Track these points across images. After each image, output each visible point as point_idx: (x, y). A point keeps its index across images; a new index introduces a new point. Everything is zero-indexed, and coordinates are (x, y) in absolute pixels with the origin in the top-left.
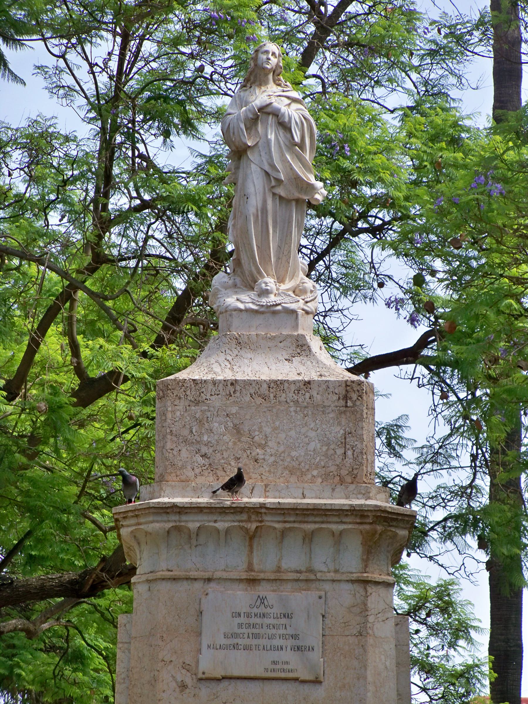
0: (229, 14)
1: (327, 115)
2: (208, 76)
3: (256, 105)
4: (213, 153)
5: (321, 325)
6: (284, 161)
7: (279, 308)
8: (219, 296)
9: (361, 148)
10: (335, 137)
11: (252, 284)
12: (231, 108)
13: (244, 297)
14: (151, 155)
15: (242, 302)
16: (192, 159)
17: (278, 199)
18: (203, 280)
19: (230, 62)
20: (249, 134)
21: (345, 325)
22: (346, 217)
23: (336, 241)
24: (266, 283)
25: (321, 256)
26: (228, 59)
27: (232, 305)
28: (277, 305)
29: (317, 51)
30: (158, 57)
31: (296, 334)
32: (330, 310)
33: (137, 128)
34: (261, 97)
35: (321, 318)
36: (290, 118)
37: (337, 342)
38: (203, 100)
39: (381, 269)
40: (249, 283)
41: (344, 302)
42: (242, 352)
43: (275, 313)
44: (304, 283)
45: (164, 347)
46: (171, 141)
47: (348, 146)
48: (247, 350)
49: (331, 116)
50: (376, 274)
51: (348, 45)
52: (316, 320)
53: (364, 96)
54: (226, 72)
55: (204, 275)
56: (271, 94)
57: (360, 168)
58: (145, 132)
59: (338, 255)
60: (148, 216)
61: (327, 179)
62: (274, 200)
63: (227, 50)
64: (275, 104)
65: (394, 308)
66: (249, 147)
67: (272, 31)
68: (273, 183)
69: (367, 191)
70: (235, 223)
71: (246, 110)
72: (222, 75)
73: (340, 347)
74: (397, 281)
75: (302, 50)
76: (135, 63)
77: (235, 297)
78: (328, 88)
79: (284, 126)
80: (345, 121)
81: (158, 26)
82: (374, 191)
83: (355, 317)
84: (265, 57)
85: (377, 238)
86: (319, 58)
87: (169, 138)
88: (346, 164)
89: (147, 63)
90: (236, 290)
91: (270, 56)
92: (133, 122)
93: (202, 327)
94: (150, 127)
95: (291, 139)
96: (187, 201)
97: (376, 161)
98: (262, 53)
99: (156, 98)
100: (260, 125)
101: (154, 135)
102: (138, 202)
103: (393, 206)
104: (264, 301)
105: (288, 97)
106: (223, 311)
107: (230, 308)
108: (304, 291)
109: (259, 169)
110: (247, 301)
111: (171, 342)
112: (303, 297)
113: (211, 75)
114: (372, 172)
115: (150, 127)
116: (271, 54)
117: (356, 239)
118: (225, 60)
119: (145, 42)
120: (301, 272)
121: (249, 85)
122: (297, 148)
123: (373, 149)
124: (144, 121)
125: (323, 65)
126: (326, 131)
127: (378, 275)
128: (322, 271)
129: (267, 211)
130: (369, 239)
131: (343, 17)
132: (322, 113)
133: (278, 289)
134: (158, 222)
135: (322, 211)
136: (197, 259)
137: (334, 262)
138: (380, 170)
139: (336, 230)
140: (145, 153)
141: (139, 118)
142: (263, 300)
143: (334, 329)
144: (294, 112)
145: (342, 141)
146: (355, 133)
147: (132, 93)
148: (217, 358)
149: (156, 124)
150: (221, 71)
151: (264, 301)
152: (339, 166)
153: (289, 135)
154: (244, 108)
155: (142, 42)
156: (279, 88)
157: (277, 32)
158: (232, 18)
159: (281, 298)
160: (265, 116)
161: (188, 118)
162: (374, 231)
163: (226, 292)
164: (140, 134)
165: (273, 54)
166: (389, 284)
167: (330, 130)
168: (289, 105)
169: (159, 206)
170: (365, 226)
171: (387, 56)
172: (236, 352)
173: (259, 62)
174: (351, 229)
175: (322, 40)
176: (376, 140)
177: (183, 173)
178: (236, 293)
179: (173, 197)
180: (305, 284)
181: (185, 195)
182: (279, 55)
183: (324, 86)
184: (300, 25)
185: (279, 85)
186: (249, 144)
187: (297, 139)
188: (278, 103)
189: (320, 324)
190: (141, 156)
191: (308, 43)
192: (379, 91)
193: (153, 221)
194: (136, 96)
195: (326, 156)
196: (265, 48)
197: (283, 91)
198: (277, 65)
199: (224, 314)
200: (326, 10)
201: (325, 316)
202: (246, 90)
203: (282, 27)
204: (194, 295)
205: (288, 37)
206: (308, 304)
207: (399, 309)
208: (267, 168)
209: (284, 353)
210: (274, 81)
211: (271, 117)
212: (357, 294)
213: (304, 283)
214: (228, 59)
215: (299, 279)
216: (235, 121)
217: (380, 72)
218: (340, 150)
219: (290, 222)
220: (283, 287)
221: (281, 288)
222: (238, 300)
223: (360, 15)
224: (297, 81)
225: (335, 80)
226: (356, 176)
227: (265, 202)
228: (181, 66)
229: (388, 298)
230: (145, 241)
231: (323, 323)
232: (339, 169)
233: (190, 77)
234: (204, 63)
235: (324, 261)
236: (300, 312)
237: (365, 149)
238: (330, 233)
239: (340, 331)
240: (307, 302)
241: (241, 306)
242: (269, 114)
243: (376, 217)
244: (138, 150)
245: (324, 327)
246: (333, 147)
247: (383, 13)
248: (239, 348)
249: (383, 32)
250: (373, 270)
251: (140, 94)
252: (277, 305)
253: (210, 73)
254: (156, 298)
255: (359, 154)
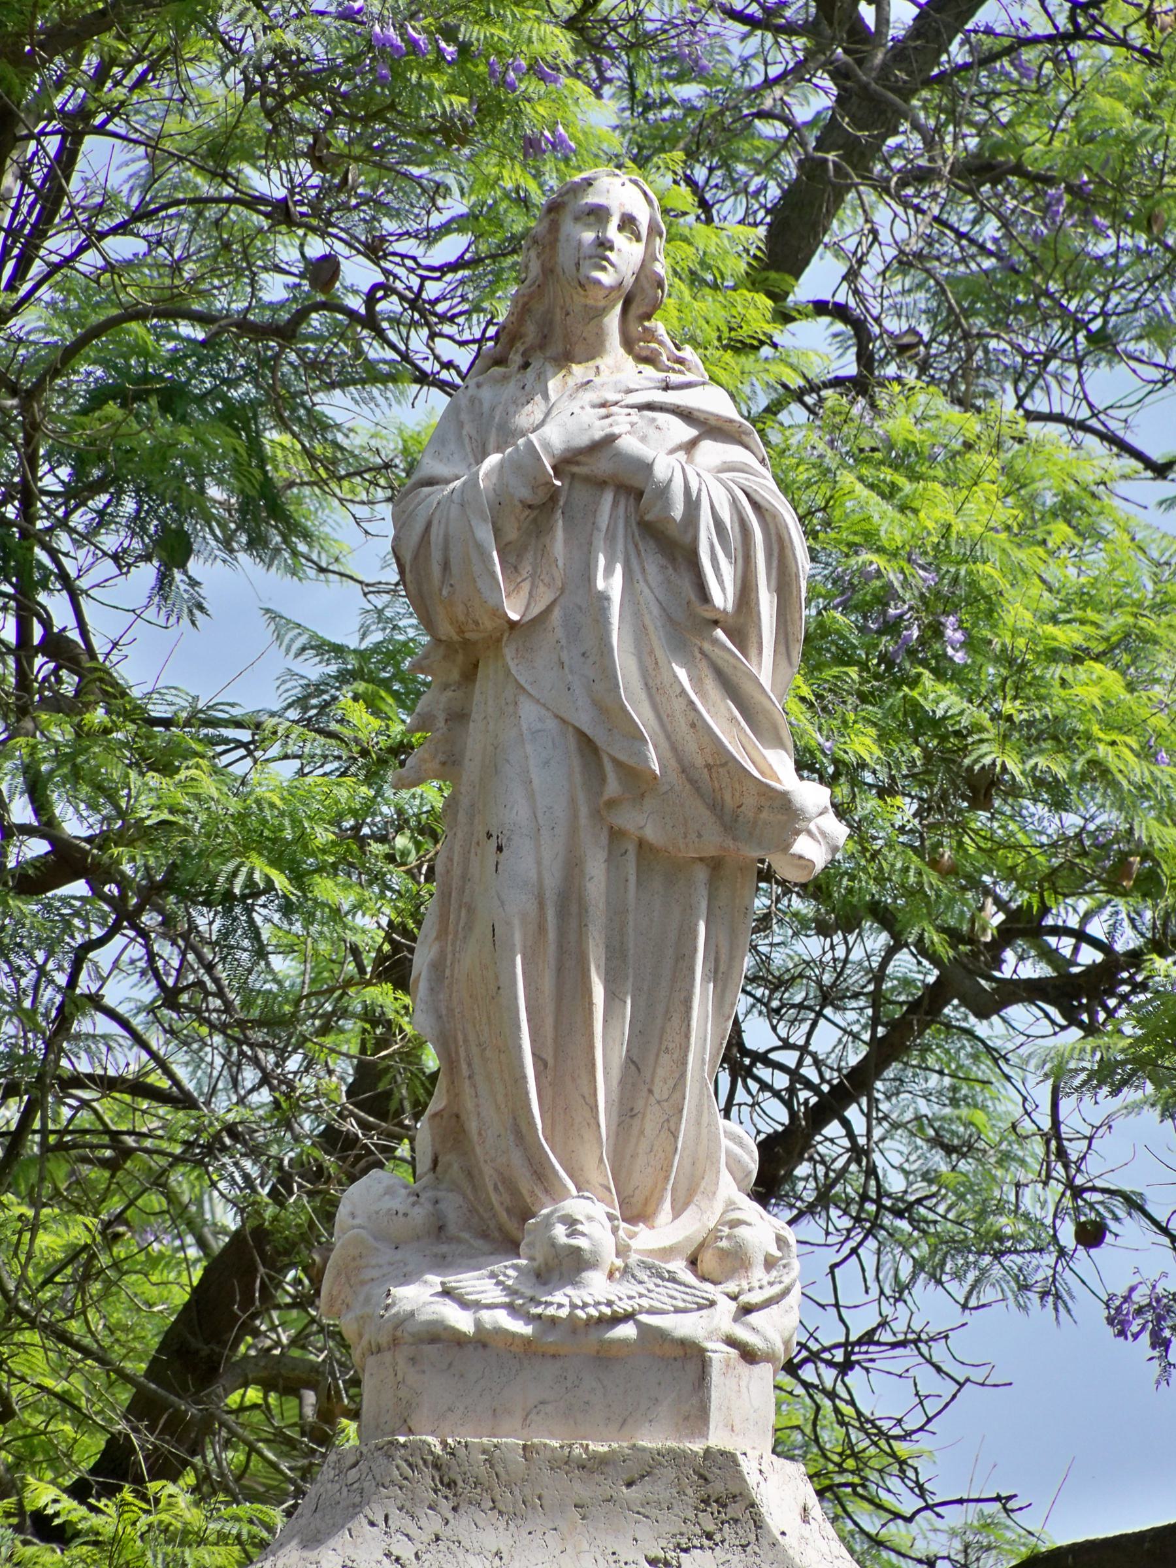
0: (449, 33)
1: (871, 487)
2: (356, 303)
3: (547, 446)
4: (376, 637)
5: (826, 1403)
6: (656, 688)
7: (627, 1331)
8: (369, 1274)
9: (1016, 633)
10: (905, 583)
11: (511, 1226)
12: (437, 454)
13: (476, 1283)
14: (100, 645)
15: (464, 1304)
16: (279, 661)
17: (632, 856)
18: (310, 1194)
19: (451, 247)
20: (511, 568)
21: (932, 1407)
22: (942, 929)
23: (900, 1033)
24: (571, 1222)
25: (831, 1106)
26: (445, 229)
27: (424, 1316)
28: (617, 1319)
29: (839, 200)
30: (142, 214)
31: (697, 1447)
32: (868, 1338)
33: (40, 525)
34: (565, 412)
35: (829, 1376)
36: (692, 505)
37: (894, 1483)
38: (335, 405)
39: (1093, 1166)
40: (492, 1218)
41: (931, 1305)
42: (461, 1526)
43: (607, 1358)
44: (735, 1224)
45: (127, 1494)
46: (194, 583)
47: (960, 626)
48: (480, 1516)
49: (889, 492)
50: (1070, 1184)
51: (980, 171)
52: (806, 1385)
53: (1038, 402)
54: (432, 289)
55: (319, 1174)
56: (612, 397)
57: (1009, 718)
58: (77, 545)
59: (913, 1093)
60: (77, 913)
61: (863, 765)
62: (614, 857)
63: (441, 190)
64: (629, 444)
65: (1145, 1337)
66: (513, 625)
67: (648, 107)
68: (613, 787)
69: (1043, 822)
70: (442, 954)
71: (501, 464)
72: (415, 302)
73: (909, 1503)
74: (1162, 1218)
75: (774, 192)
76: (43, 236)
77: (435, 1281)
78: (883, 362)
79: (665, 542)
80: (950, 517)
81: (152, 68)
82: (1072, 821)
83: (978, 1375)
84: (589, 236)
85: (1080, 1025)
86: (845, 227)
87: (182, 566)
88: (942, 698)
89: (92, 239)
90: (444, 1248)
91: (612, 232)
92: (27, 495)
93: (310, 1397)
94: (103, 518)
95: (693, 596)
96: (244, 849)
97: (1078, 690)
98: (577, 219)
99: (125, 391)
100: (559, 533)
101: (115, 557)
102: (38, 847)
103: (1149, 885)
104: (561, 1301)
105: (686, 415)
106: (384, 1340)
107: (410, 1327)
108: (736, 1260)
109: (551, 724)
110: (486, 1299)
111: (168, 1470)
112: (731, 1287)
113: (371, 299)
114: (1057, 734)
115: (103, 518)
116: (615, 221)
117: (989, 1029)
118: (431, 237)
119: (89, 141)
120: (726, 1178)
121: (516, 359)
122: (719, 633)
123: (1067, 636)
124: (76, 493)
125: (861, 262)
126: (866, 556)
127: (1078, 1192)
128: (839, 1164)
129: (583, 910)
130: (1045, 1027)
131: (957, 52)
132: (847, 479)
133: (622, 1251)
134: (118, 941)
135: (838, 905)
136: (284, 1113)
137: (895, 1126)
138: (1095, 729)
139: (906, 982)
140: (74, 635)
141: (53, 478)
142: (558, 1297)
143: (885, 1425)
144: (710, 480)
145: (937, 603)
146: (988, 568)
147: (20, 372)
148: (350, 1551)
149: (129, 505)
150: (415, 282)
151: (561, 1301)
152: (916, 705)
153: (686, 585)
154: (494, 459)
155: (78, 141)
156: (649, 370)
157: (666, 112)
158: (464, 49)
159: (634, 1289)
160: (582, 494)
161: (268, 481)
162: (1074, 995)
163: (399, 1255)
164: (53, 554)
165: (628, 223)
166: (1129, 1231)
167: (880, 550)
168: (690, 446)
169: (127, 868)
170: (1033, 970)
171: (1149, 222)
172: (432, 1523)
173: (565, 258)
174: (968, 978)
175: (859, 156)
176: (1085, 598)
177: (238, 724)
178: (442, 1264)
179: (186, 831)
180: (742, 1231)
181: (241, 818)
182: (654, 230)
183: (865, 359)
184: (769, 83)
185: (649, 359)
186: (515, 617)
187: (723, 596)
188: (643, 439)
189: (819, 1397)
190: (55, 646)
191: (801, 165)
192: (1108, 382)
193: (97, 932)
194: (39, 386)
195: (864, 666)
196: (592, 198)
197: (667, 388)
198: (644, 270)
199: (387, 1357)
200: (882, 19)
201: (845, 1367)
202: (505, 378)
203: (690, 91)
204: (269, 1263)
205: (713, 137)
206: (753, 1318)
207: (1166, 1344)
208: (584, 720)
209: (644, 1531)
210: (628, 344)
211: (608, 498)
212: (984, 1271)
213: (735, 1224)
214: (445, 229)
215: (719, 1207)
216: (455, 510)
217: (1115, 298)
218: (922, 640)
219: (685, 958)
220: (646, 1239)
221: (634, 1244)
222: (447, 1293)
223: (1036, 40)
224: (742, 334)
225: (912, 331)
226: (988, 754)
227: (573, 866)
228: (238, 259)
229: (1122, 1291)
230: (63, 1019)
231: (832, 1395)
232: (921, 722)
233: (282, 304)
234: (339, 247)
235: (846, 1124)
236: (719, 1353)
237: (1034, 639)
238: (877, 999)
239: (906, 1436)
240: (747, 1310)
241: (462, 1321)
242: (600, 484)
243: (1081, 936)
244: (47, 623)
245: (837, 1410)
246: (892, 627)
247: (1137, 34)
248: (445, 1506)
249: (1130, 124)
250: (1059, 1170)
251: (57, 373)
252: (617, 1319)
253: (366, 289)
254: (116, 1264)
255: (1006, 658)
